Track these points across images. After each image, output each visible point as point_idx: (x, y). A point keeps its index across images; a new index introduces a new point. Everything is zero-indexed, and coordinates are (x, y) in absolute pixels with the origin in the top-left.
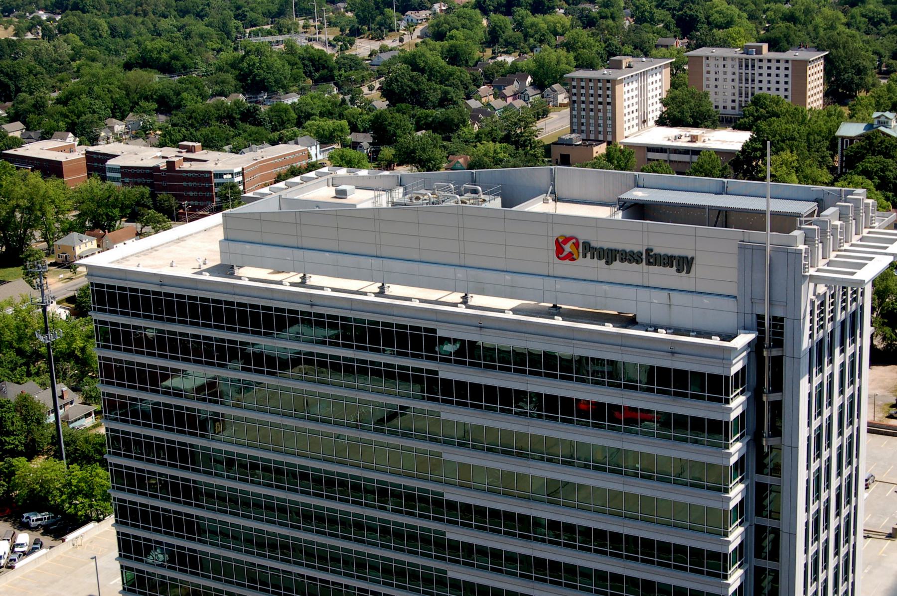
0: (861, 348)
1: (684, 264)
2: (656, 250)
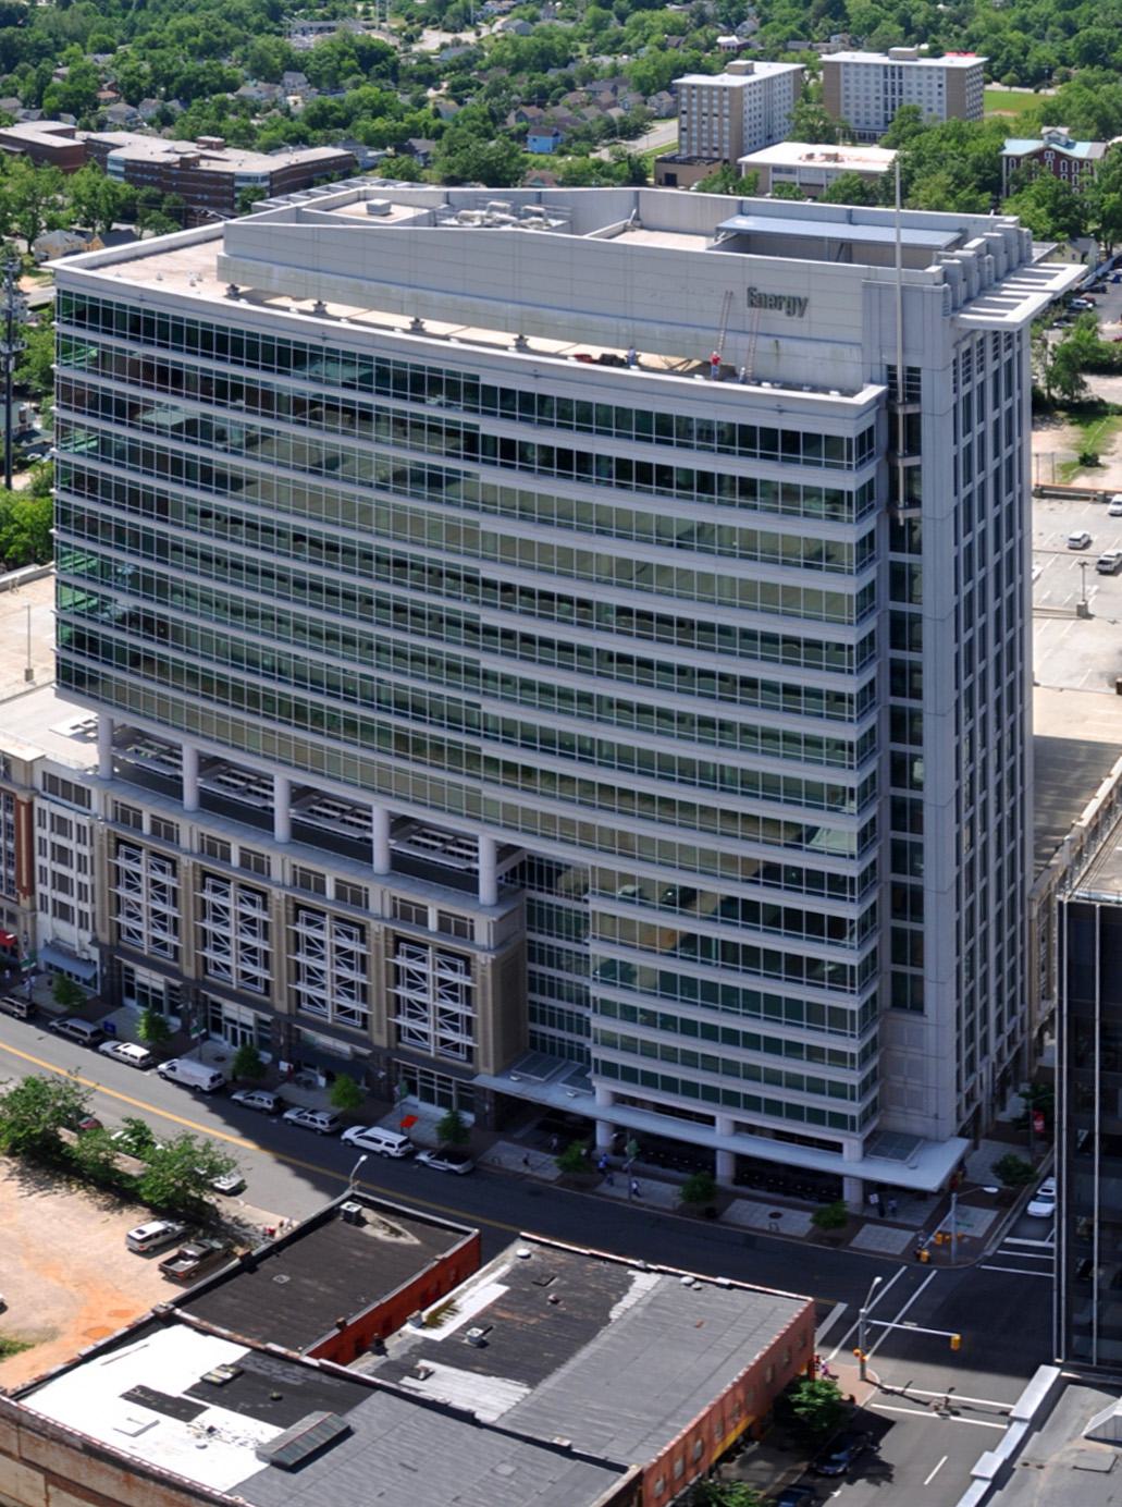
0: (1020, 402)
1: (796, 305)
2: (761, 290)
